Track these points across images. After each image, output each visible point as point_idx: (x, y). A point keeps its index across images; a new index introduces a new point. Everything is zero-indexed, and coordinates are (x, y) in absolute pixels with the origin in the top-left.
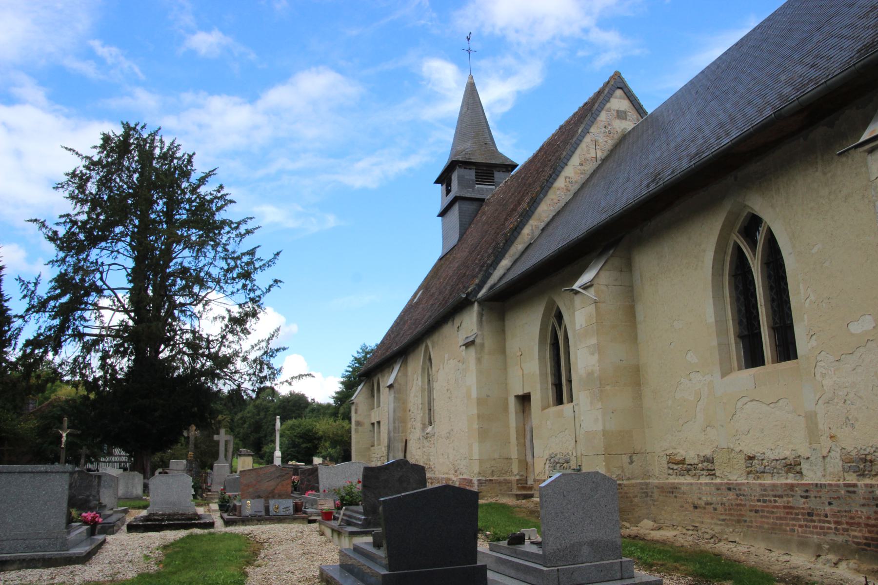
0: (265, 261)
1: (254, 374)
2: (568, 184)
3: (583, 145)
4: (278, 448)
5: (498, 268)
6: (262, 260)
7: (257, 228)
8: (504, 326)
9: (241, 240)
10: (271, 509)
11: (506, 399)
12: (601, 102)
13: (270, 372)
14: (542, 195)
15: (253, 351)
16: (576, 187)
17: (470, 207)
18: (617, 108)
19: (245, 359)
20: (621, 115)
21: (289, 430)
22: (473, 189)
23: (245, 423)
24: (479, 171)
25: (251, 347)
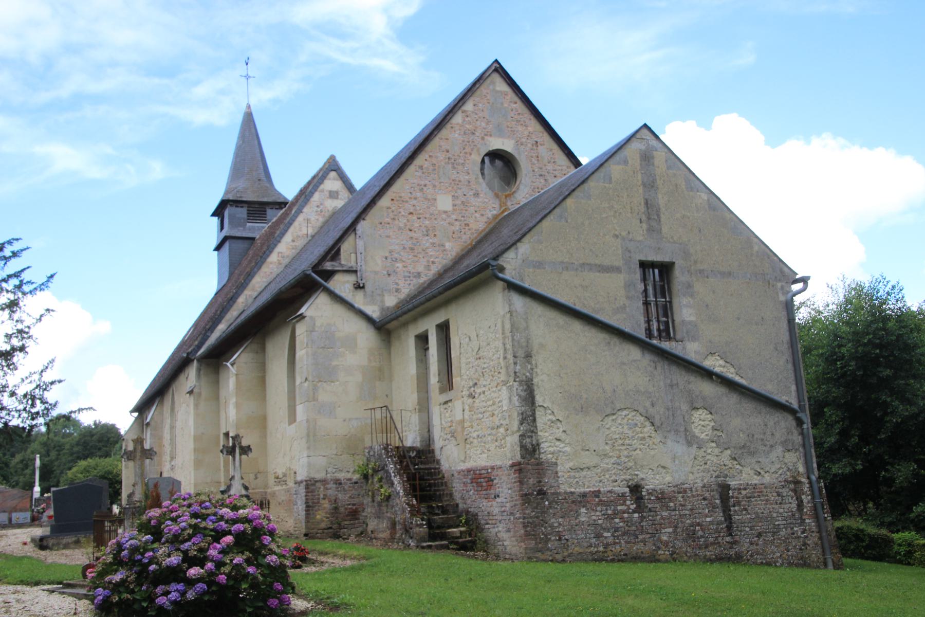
0: (37, 285)
1: (25, 409)
2: (280, 258)
3: (296, 224)
4: (37, 483)
5: (215, 331)
6: (33, 283)
7: (25, 249)
8: (218, 378)
9: (6, 263)
10: (13, 519)
11: (219, 435)
12: (315, 185)
13: (43, 408)
14: (255, 269)
15: (23, 384)
16: (287, 261)
17: (242, 245)
18: (330, 189)
19: (13, 394)
20: (333, 195)
21: (81, 473)
22: (244, 228)
23: (27, 468)
24: (251, 209)
25: (20, 380)
